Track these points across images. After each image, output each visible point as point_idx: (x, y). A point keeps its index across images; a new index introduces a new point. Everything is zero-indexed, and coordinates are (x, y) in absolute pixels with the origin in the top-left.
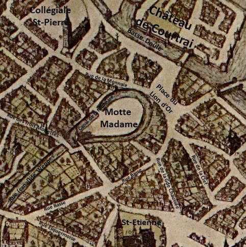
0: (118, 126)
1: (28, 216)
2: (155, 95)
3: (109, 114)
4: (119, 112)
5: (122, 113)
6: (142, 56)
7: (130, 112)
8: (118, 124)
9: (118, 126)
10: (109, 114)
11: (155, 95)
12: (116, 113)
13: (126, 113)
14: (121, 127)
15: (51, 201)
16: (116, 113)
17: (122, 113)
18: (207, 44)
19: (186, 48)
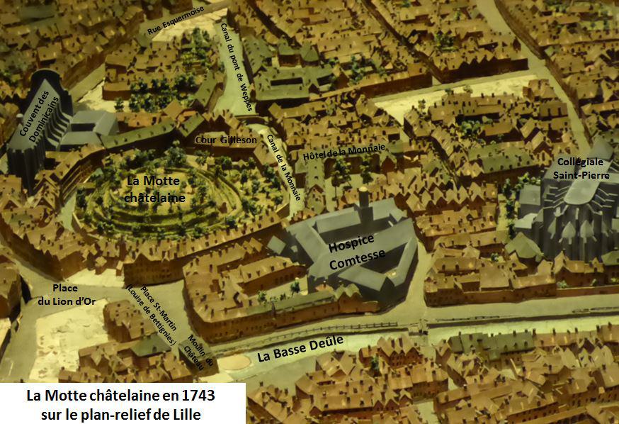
0: (159, 418)
1: (547, 78)
2: (61, 300)
3: (52, 399)
4: (68, 395)
5: (72, 396)
6: (241, 40)
7: (199, 415)
8: (159, 413)
9: (159, 418)
10: (52, 399)
11: (61, 300)
12: (63, 397)
13: (172, 182)
14: (283, 356)
15: (555, 394)
16: (63, 397)
17: (72, 396)
18: (544, 19)
19: (47, 124)
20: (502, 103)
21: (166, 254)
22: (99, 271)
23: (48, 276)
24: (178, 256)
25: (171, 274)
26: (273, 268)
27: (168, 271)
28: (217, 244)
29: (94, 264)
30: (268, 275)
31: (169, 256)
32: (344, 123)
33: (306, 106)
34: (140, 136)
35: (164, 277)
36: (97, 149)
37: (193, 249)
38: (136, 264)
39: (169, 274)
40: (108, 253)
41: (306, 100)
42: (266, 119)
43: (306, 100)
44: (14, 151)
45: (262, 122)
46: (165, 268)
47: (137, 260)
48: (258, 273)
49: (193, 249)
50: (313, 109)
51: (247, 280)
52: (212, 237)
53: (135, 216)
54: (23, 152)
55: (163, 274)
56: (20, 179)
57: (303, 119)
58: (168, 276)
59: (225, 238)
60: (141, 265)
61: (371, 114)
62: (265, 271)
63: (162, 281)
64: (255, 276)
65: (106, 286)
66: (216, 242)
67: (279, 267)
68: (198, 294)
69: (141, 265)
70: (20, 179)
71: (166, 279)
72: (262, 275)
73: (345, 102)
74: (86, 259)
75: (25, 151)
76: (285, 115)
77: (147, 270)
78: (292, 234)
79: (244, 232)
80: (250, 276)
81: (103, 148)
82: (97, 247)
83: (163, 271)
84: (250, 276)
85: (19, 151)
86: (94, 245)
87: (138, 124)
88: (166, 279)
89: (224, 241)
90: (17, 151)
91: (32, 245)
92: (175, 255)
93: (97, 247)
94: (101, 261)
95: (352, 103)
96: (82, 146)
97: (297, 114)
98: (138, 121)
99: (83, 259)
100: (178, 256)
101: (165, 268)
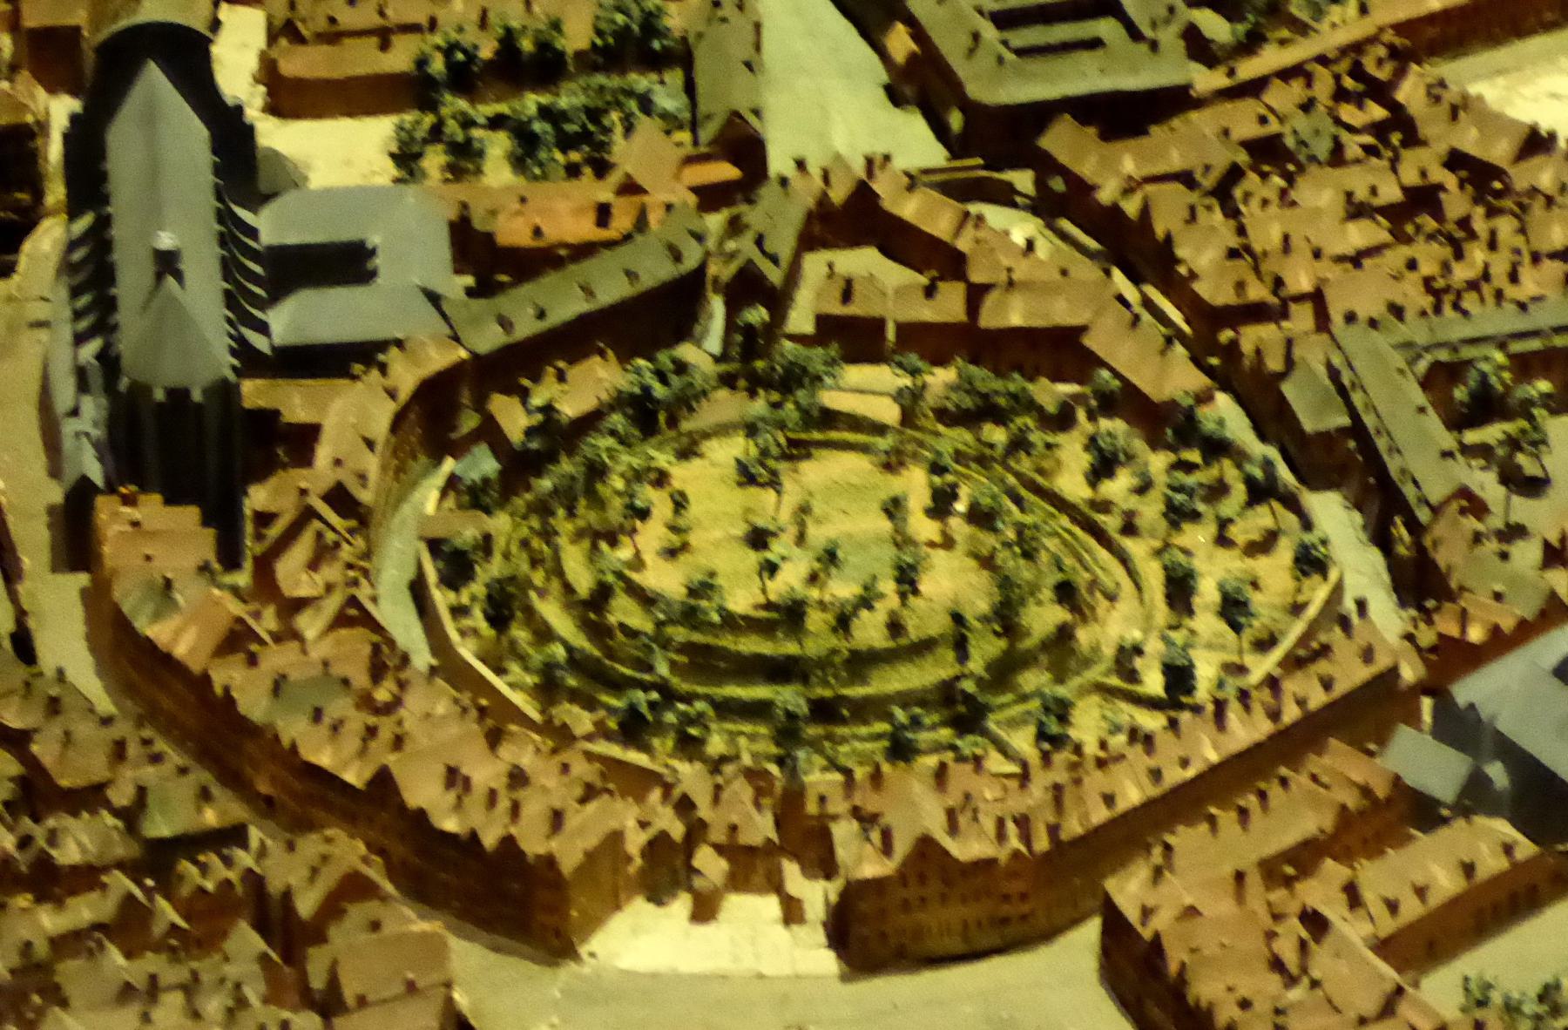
20: (1444, 108)
21: (1011, 828)
22: (704, 911)
23: (502, 941)
24: (1064, 836)
25: (1032, 913)
26: (1468, 869)
27: (1024, 897)
28: (1190, 773)
29: (689, 878)
30: (1454, 903)
31: (1026, 838)
32: (1390, 193)
33: (1203, 122)
34: (588, 292)
35: (1005, 921)
36: (440, 358)
37: (1109, 800)
38: (902, 877)
39: (1025, 908)
40: (734, 828)
41: (1174, 101)
42: (1023, 180)
43: (1174, 101)
44: (159, 395)
45: (1005, 196)
46: (1016, 886)
47: (907, 863)
48: (1421, 892)
49: (1109, 800)
50: (1226, 132)
51: (1387, 925)
52: (1169, 749)
53: (759, 658)
54: (197, 396)
55: (1006, 910)
56: (1334, 743)
57: (1208, 182)
58: (1024, 918)
59: (1216, 747)
60: (922, 879)
61: (1499, 152)
62: (1446, 883)
63: (993, 940)
64: (1412, 909)
65: (767, 971)
66: (1185, 763)
67: (1491, 864)
68: (1245, 1004)
69: (922, 879)
70: (1334, 743)
71: (1011, 931)
72: (1435, 899)
73: (1358, 100)
74: (638, 861)
75: (206, 392)
76: (1129, 166)
77: (944, 898)
78: (1484, 715)
79: (1274, 715)
80: (1393, 907)
81: (463, 354)
82: (685, 806)
83: (1006, 898)
84: (1393, 907)
85: (178, 395)
86: (1090, 931)
87: (537, 232)
88: (1011, 931)
89: (1214, 757)
90: (172, 393)
91: (421, 815)
92: (1053, 830)
93: (685, 806)
94: (710, 865)
95: (565, 134)
96: (383, 346)
97: (1175, 160)
98: (538, 221)
99: (629, 859)
100: (1064, 836)
101: (1016, 886)
